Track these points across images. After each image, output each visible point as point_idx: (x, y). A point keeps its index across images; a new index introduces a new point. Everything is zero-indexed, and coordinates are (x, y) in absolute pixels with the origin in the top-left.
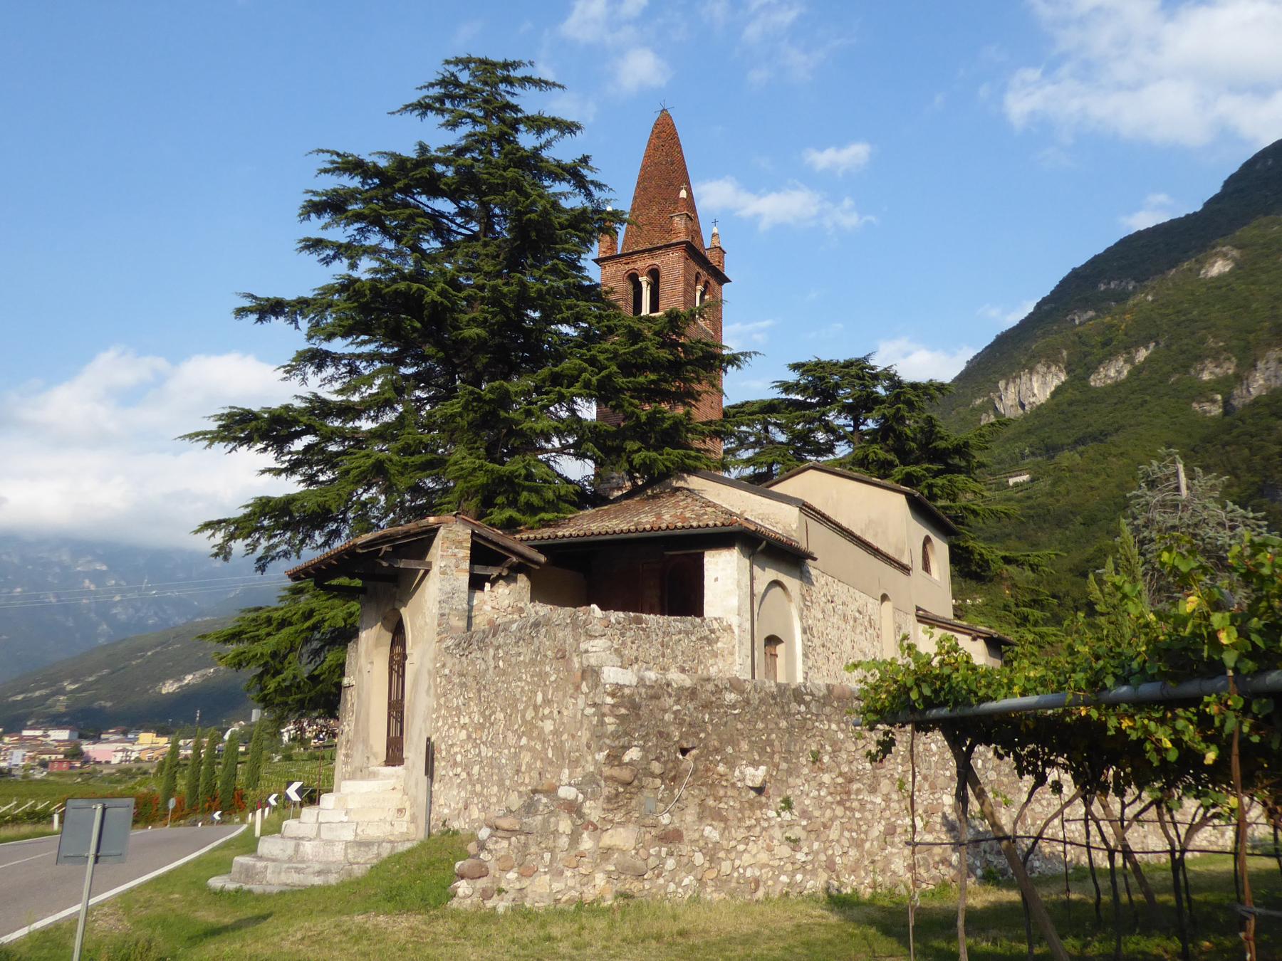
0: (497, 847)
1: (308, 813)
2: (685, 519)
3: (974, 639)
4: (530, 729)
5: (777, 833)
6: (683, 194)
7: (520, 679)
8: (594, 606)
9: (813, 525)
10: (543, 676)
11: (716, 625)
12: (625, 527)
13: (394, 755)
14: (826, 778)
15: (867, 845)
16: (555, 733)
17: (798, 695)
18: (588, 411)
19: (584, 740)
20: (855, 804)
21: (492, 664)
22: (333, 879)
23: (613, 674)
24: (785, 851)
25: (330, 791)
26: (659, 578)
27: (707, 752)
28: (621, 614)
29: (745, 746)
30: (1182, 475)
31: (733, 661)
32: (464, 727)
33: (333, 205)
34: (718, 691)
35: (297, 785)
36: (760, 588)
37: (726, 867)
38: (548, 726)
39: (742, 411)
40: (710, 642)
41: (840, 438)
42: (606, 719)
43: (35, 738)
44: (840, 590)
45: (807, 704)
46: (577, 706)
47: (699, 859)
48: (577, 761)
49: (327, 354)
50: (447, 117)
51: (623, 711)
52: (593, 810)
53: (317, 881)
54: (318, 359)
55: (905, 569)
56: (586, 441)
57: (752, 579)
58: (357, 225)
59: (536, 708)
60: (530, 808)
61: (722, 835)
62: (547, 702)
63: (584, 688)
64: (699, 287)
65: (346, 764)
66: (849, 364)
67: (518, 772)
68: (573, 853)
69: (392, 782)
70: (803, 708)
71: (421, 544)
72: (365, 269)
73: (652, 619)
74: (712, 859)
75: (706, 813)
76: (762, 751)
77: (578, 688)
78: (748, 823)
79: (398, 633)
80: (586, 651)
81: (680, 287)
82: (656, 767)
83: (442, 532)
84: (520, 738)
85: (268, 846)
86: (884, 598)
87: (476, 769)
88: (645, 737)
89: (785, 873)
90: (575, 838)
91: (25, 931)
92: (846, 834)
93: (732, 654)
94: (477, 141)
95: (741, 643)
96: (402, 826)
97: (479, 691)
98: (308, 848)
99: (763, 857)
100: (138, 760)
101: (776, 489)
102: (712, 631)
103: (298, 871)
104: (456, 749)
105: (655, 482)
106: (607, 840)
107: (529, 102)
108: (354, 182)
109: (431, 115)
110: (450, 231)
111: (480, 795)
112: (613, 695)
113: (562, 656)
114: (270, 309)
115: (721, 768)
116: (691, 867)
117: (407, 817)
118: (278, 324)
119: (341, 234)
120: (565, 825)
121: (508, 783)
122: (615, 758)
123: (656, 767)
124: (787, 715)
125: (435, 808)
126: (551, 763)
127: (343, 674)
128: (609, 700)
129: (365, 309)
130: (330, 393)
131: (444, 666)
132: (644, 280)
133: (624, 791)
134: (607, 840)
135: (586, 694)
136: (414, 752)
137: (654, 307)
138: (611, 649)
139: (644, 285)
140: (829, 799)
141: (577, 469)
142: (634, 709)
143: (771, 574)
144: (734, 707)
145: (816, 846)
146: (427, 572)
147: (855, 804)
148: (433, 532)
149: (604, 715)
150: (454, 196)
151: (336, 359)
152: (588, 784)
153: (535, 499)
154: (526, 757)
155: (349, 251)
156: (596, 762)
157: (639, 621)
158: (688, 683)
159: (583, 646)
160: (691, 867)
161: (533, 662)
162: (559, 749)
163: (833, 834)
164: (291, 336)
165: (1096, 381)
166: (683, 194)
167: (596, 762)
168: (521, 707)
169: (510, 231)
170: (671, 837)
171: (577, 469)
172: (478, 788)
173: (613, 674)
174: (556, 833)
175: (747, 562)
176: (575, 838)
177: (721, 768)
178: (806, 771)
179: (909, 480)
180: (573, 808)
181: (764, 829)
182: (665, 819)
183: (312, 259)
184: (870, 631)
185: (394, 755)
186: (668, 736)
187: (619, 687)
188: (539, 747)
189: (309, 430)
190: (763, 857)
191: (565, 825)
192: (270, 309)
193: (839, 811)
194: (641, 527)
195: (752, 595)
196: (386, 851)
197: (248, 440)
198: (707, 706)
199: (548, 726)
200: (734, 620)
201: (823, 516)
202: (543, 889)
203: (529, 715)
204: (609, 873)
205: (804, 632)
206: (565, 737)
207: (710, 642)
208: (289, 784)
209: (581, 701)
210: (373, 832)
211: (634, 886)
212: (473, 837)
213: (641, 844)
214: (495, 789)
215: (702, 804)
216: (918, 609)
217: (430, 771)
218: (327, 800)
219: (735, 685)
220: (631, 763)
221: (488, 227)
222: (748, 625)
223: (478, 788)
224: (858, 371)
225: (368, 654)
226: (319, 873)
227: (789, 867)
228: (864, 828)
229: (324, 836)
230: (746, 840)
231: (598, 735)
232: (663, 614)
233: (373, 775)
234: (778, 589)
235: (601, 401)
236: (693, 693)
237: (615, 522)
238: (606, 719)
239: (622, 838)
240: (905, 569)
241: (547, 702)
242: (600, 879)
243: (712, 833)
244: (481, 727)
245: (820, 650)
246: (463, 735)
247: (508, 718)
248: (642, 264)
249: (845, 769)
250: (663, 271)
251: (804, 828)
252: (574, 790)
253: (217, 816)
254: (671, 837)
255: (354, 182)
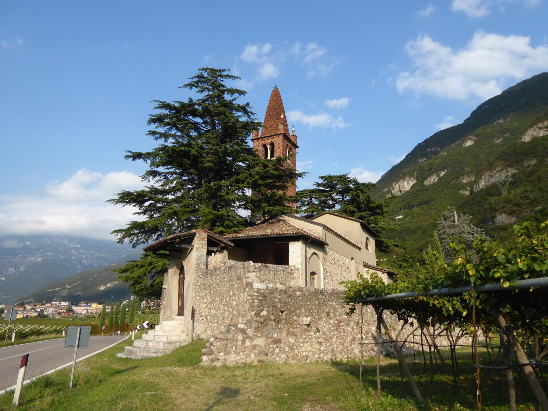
0: (217, 344)
1: (151, 332)
2: (282, 231)
3: (383, 273)
4: (228, 304)
5: (314, 340)
6: (282, 116)
7: (225, 287)
8: (251, 261)
9: (327, 233)
10: (233, 285)
11: (293, 268)
12: (261, 234)
13: (181, 313)
14: (331, 321)
15: (346, 344)
16: (237, 305)
17: (322, 293)
18: (249, 193)
19: (247, 308)
20: (342, 330)
21: (215, 281)
22: (159, 355)
23: (257, 285)
24: (317, 346)
25: (158, 324)
26: (273, 251)
27: (290, 312)
28: (260, 264)
29: (303, 310)
30: (456, 216)
31: (299, 281)
32: (205, 303)
33: (159, 120)
34: (294, 291)
35: (146, 322)
36: (309, 255)
37: (296, 352)
38: (234, 303)
39: (303, 193)
40: (291, 274)
41: (337, 203)
42: (255, 301)
43: (56, 304)
44: (336, 256)
45: (325, 296)
46: (245, 296)
47: (287, 349)
48: (245, 315)
49: (157, 172)
50: (199, 89)
51: (261, 298)
52: (250, 332)
53: (154, 355)
54: (154, 174)
55: (360, 249)
56: (247, 203)
57: (306, 252)
58: (167, 127)
59: (230, 297)
60: (228, 331)
61: (295, 341)
62: (234, 295)
63: (247, 290)
64: (288, 149)
65: (164, 315)
66: (340, 177)
67: (224, 319)
68: (243, 347)
69: (180, 322)
70: (323, 297)
71: (190, 239)
72: (170, 143)
73: (271, 266)
74: (292, 349)
75: (289, 333)
76: (309, 312)
77: (245, 290)
78: (304, 337)
79: (182, 270)
80: (248, 277)
81: (281, 149)
82: (272, 317)
83: (197, 235)
84: (225, 307)
85: (137, 343)
86: (352, 259)
87: (209, 317)
88: (268, 307)
89: (317, 354)
90: (244, 341)
91: (54, 370)
92: (338, 340)
93: (299, 278)
94: (209, 97)
95: (302, 274)
96: (183, 337)
97: (210, 290)
98: (151, 344)
99: (309, 348)
100: (91, 313)
101: (314, 220)
102: (292, 270)
103: (147, 352)
104: (202, 311)
105: (273, 217)
106: (255, 342)
107: (228, 84)
108: (167, 112)
109: (194, 88)
110: (200, 129)
111: (210, 326)
112: (257, 292)
113: (239, 279)
114: (137, 156)
115: (295, 318)
116: (284, 352)
117: (185, 334)
118: (140, 161)
119: (162, 130)
120: (240, 337)
121: (220, 322)
122: (258, 314)
123: (272, 317)
124: (318, 299)
125: (195, 331)
126: (235, 316)
127: (162, 284)
128: (256, 294)
129: (170, 157)
130: (158, 186)
131: (198, 282)
132: (268, 147)
133: (261, 326)
134: (255, 342)
135: (248, 292)
136: (187, 312)
137: (272, 156)
138: (257, 276)
139: (268, 148)
140: (332, 328)
141: (245, 213)
142: (264, 297)
143: (313, 250)
144: (299, 296)
145: (328, 344)
146: (192, 249)
147: (342, 330)
148: (194, 235)
149: (254, 299)
150: (202, 117)
151: (160, 174)
152: (248, 323)
153: (230, 224)
154: (227, 314)
155: (165, 136)
156: (251, 315)
157: (266, 267)
158: (283, 288)
159: (247, 275)
160: (284, 352)
161: (229, 281)
162: (238, 311)
163: (334, 340)
164: (145, 166)
165: (426, 183)
166: (282, 116)
167: (251, 315)
168: (225, 296)
169: (221, 129)
170: (277, 341)
171: (245, 213)
172: (210, 324)
173: (257, 285)
174: (237, 340)
175: (304, 246)
176: (244, 341)
177: (295, 318)
178: (324, 319)
179: (361, 217)
180: (243, 331)
181: (310, 339)
182: (275, 335)
183: (152, 138)
184: (347, 270)
185: (181, 313)
186: (276, 307)
187: (260, 290)
188: (231, 310)
189: (151, 199)
190: (309, 348)
191: (240, 337)
192: (137, 156)
193: (336, 332)
194: (267, 234)
195: (306, 258)
196: (178, 345)
197: (129, 202)
198: (290, 296)
199: (234, 303)
200: (300, 267)
201: (331, 230)
202: (233, 359)
203: (228, 299)
204: (256, 354)
205: (324, 270)
206: (240, 307)
207: (291, 274)
208: (144, 322)
209: (246, 294)
210: (173, 339)
211: (264, 358)
212: (208, 341)
213: (267, 344)
214: (216, 324)
215: (288, 330)
216: (364, 262)
217: (193, 318)
218: (157, 327)
219: (300, 289)
220: (263, 316)
221: (214, 128)
222: (305, 268)
223: (210, 324)
224: (343, 179)
225: (171, 277)
226: (155, 352)
227: (318, 352)
228: (344, 338)
229: (156, 340)
230: (303, 342)
231: (252, 306)
232: (275, 264)
233: (173, 319)
234: (315, 256)
235: (253, 189)
236: (285, 292)
237: (258, 232)
238: (255, 301)
239: (260, 341)
240: (360, 249)
241: (234, 295)
242: (252, 356)
243: (291, 340)
244: (211, 303)
245: (330, 277)
246: (205, 306)
247: (220, 300)
248: (268, 141)
249: (338, 318)
250: (275, 144)
251: (324, 338)
252: (243, 325)
253: (119, 332)
254: (277, 341)
255: (167, 112)
